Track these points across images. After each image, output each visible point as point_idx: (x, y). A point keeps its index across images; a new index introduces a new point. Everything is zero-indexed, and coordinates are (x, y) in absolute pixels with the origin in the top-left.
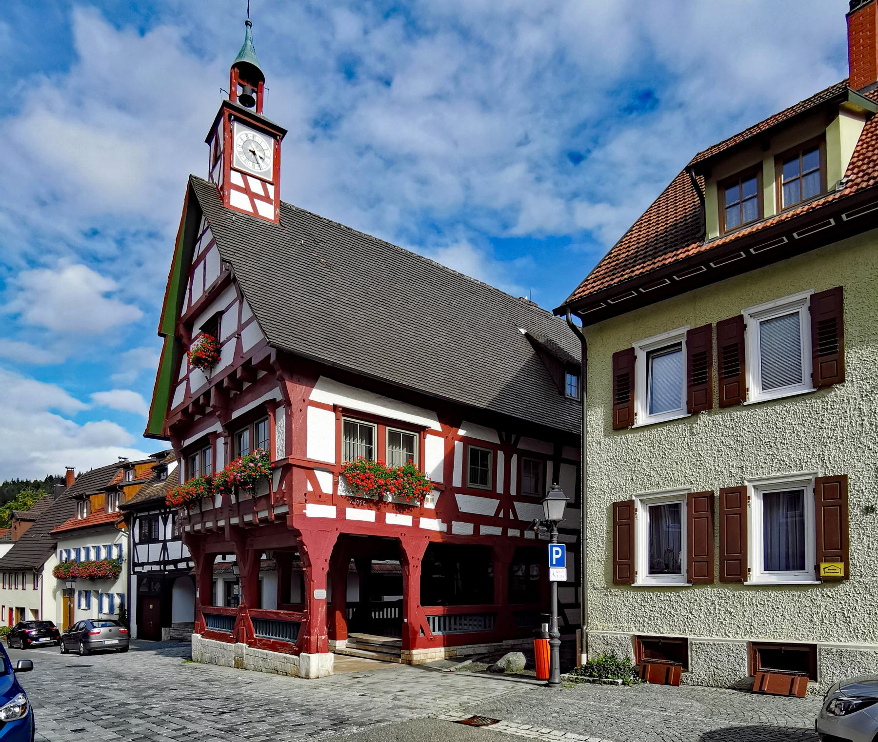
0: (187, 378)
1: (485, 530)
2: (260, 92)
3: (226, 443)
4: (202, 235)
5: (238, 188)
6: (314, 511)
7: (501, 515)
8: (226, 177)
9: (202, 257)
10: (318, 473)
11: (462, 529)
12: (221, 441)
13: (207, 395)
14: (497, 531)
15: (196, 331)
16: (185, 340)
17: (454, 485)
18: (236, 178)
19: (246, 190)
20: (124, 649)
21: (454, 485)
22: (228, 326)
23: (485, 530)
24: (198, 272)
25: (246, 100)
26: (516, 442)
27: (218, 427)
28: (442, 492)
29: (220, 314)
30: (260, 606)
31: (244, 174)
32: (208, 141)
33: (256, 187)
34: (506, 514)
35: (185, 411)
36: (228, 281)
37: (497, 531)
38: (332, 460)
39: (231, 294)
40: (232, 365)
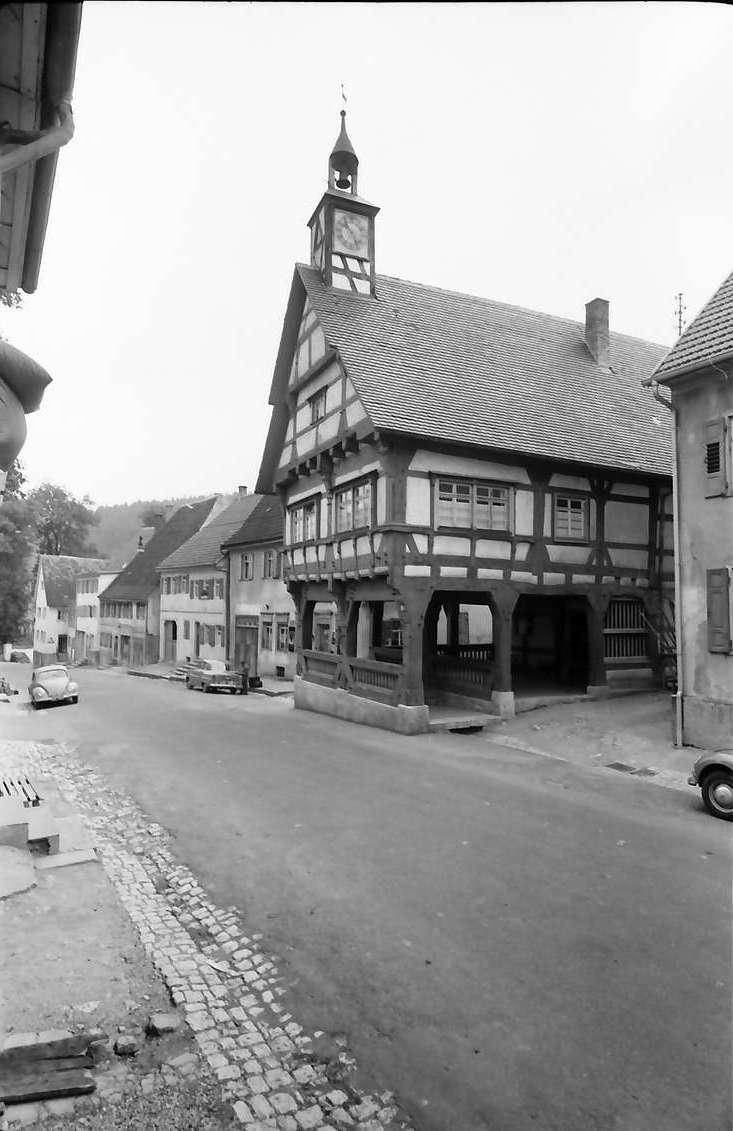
0: (294, 443)
1: (577, 578)
2: (354, 173)
3: (329, 504)
4: (307, 315)
5: (337, 270)
6: (411, 570)
7: (594, 563)
8: (329, 261)
9: (308, 335)
10: (415, 536)
11: (552, 578)
12: (324, 502)
13: (313, 460)
14: (591, 579)
15: (303, 397)
16: (290, 408)
17: (439, 643)
18: (337, 262)
19: (345, 271)
20: (243, 692)
21: (439, 643)
22: (334, 397)
23: (577, 578)
24: (304, 349)
25: (343, 184)
26: (610, 487)
27: (322, 488)
28: (532, 544)
29: (326, 387)
30: (356, 656)
31: (343, 256)
32: (310, 225)
33: (353, 265)
34: (600, 560)
35: (292, 472)
36: (332, 358)
37: (591, 579)
38: (427, 523)
39: (335, 371)
40: (337, 437)
